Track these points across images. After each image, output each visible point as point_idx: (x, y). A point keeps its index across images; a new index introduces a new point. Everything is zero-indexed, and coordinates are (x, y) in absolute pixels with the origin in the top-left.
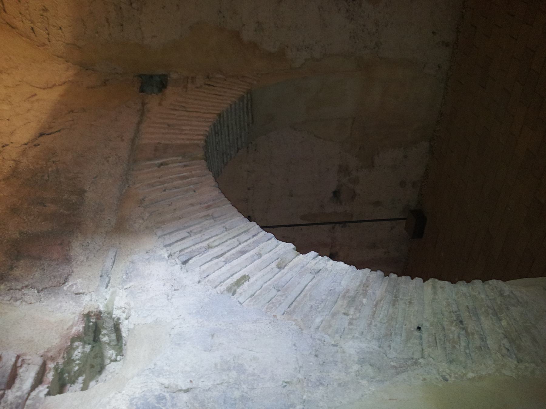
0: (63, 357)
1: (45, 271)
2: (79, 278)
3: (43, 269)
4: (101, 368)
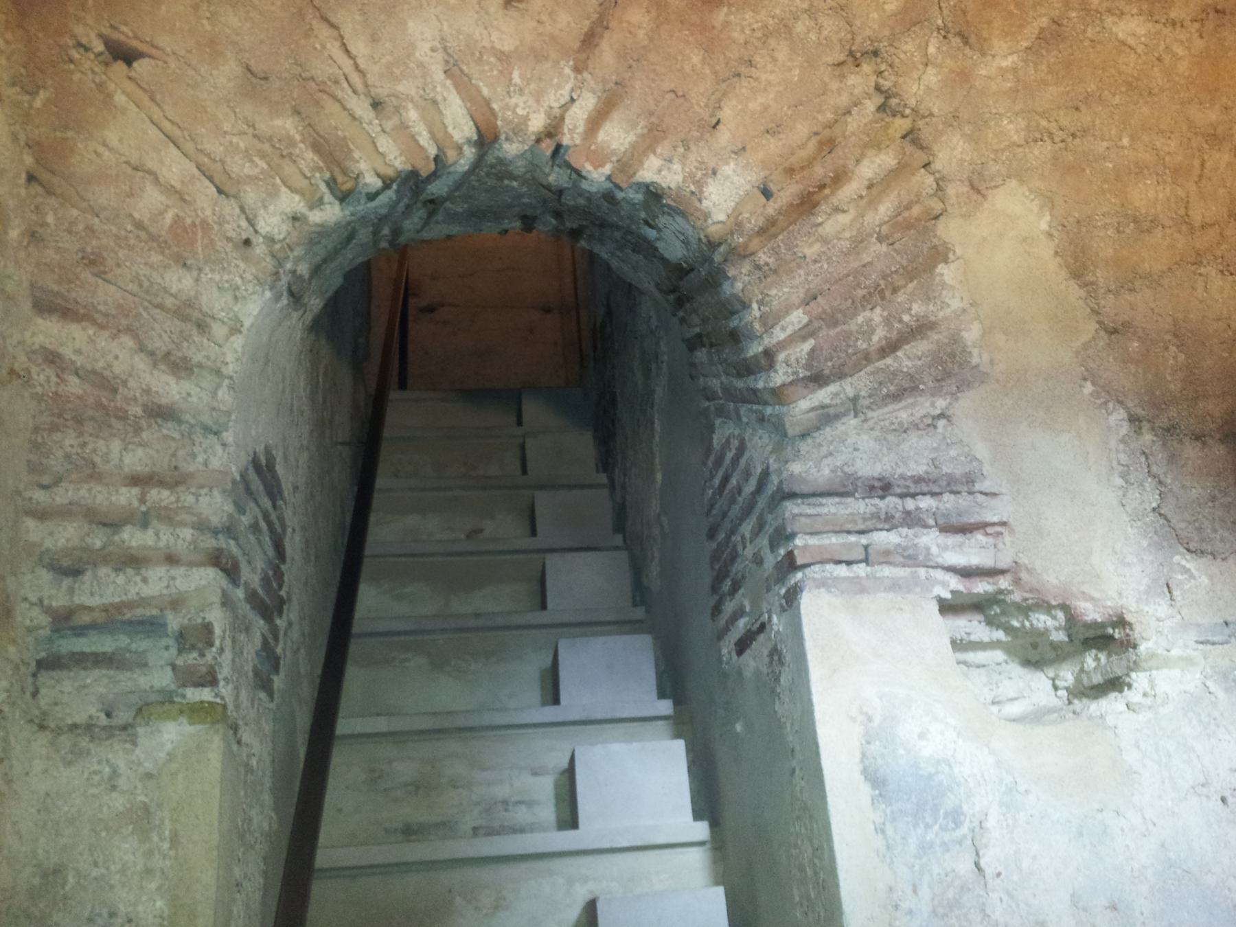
0: (1026, 599)
1: (1210, 504)
2: (1211, 578)
3: (1213, 499)
4: (1037, 662)
